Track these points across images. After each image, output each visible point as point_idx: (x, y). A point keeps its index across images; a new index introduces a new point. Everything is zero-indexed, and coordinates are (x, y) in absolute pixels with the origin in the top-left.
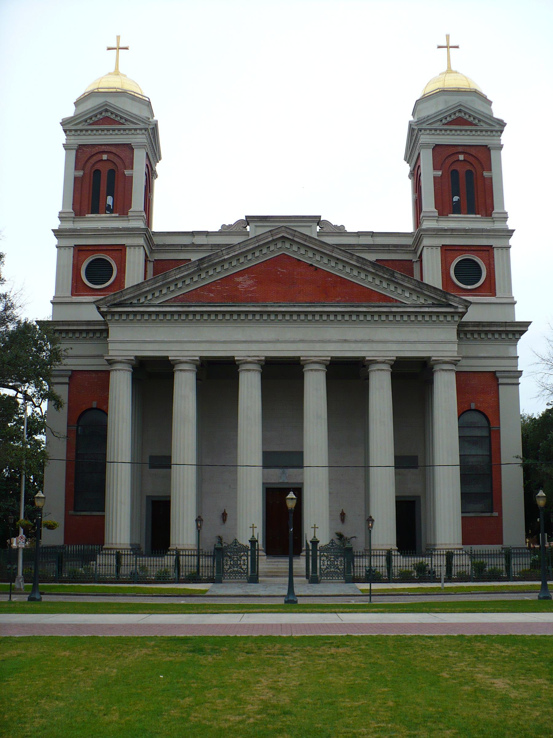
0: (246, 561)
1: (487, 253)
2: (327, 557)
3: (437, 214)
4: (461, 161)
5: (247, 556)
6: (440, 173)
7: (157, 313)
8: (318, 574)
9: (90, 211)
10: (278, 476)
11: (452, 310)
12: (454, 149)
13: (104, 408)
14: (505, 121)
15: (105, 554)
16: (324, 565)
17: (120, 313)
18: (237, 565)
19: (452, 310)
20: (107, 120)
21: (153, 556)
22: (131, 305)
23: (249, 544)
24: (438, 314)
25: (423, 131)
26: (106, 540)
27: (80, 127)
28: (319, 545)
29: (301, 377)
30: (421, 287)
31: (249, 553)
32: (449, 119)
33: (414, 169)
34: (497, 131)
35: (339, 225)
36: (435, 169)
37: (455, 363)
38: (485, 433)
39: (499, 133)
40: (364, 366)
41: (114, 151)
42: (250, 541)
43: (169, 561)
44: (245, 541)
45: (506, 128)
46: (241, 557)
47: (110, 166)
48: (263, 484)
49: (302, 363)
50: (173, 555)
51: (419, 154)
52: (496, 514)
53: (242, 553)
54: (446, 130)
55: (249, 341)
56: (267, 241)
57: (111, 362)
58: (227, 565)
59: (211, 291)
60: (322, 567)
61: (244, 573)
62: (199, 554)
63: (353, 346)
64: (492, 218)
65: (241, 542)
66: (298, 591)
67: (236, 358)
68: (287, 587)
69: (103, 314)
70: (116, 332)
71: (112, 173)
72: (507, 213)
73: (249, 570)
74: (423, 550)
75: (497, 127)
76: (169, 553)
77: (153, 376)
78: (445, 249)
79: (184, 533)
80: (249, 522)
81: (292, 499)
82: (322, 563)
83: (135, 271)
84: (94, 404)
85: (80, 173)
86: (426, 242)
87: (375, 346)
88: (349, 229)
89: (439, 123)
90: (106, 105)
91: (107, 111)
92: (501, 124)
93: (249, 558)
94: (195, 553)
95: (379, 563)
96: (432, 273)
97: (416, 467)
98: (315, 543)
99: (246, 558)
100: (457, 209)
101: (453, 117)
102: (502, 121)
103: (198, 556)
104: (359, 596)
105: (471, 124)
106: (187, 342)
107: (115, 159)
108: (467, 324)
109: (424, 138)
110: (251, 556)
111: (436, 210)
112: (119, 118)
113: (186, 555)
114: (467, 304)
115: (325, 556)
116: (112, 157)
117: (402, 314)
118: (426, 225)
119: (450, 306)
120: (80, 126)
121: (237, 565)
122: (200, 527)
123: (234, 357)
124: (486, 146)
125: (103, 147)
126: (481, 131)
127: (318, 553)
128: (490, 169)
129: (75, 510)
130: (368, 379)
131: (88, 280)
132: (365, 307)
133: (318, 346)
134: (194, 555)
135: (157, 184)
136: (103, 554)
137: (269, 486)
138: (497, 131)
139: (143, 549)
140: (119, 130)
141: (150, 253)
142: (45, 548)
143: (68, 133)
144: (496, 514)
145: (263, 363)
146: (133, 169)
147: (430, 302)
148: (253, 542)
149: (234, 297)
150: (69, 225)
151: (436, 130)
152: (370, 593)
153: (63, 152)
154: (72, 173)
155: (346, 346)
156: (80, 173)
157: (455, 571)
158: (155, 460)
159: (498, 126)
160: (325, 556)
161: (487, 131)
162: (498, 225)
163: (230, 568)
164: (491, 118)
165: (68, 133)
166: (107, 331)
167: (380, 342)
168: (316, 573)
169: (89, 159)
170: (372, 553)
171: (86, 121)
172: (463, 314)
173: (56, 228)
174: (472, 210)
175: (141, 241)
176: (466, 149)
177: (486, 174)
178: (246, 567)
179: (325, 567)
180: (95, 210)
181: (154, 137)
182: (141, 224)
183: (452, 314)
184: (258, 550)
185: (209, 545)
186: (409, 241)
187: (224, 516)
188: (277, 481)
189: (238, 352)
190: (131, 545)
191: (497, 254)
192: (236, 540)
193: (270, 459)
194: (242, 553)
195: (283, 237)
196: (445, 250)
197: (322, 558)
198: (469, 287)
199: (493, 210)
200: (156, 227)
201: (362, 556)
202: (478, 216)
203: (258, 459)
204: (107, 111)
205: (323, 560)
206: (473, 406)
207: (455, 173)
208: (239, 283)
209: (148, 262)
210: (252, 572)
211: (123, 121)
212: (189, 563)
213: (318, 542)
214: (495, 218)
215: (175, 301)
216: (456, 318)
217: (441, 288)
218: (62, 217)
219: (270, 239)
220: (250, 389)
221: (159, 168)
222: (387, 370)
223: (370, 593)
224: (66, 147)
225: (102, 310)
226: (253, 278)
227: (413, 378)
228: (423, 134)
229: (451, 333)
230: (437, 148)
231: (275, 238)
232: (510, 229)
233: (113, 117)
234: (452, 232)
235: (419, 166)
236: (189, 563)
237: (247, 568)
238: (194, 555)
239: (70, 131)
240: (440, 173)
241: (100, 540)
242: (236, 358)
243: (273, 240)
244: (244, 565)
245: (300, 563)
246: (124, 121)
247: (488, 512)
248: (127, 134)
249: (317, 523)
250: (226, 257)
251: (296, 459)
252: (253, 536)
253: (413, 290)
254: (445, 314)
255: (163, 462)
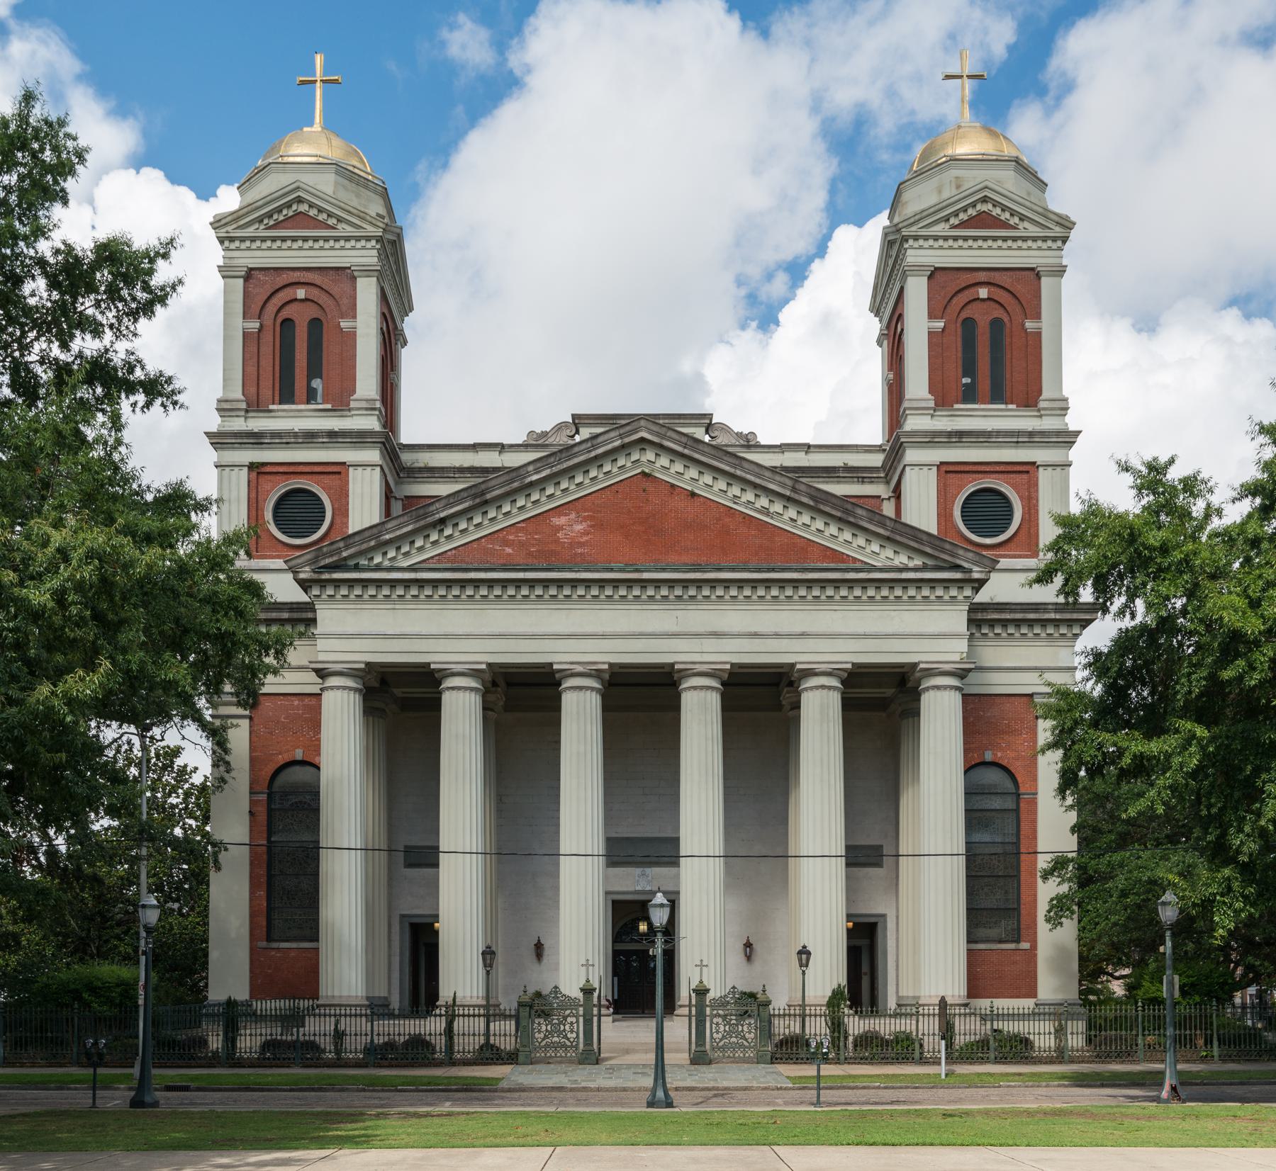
0: (574, 1028)
1: (1025, 476)
2: (724, 1017)
3: (932, 404)
4: (983, 300)
5: (577, 1017)
6: (940, 324)
7: (407, 584)
8: (708, 1046)
9: (277, 398)
10: (631, 881)
11: (958, 575)
12: (284, 279)
13: (316, 761)
14: (1072, 219)
15: (320, 1015)
16: (718, 1032)
17: (337, 583)
18: (560, 1033)
19: (958, 575)
20: (300, 220)
21: (415, 1018)
22: (357, 568)
23: (580, 995)
24: (933, 583)
25: (911, 242)
26: (322, 992)
27: (249, 232)
28: (711, 995)
29: (675, 707)
30: (900, 534)
31: (581, 1012)
32: (963, 216)
33: (888, 327)
34: (1054, 239)
35: (745, 432)
36: (932, 315)
37: (962, 674)
38: (1012, 805)
39: (1059, 243)
40: (791, 684)
41: (318, 283)
42: (582, 990)
43: (432, 1026)
44: (571, 987)
45: (1073, 234)
46: (565, 1018)
47: (313, 312)
48: (607, 893)
49: (676, 676)
50: (441, 1015)
51: (902, 289)
52: (1025, 945)
53: (568, 1012)
54: (955, 239)
55: (581, 634)
56: (610, 447)
57: (322, 674)
58: (539, 1032)
59: (506, 543)
60: (715, 1035)
61: (572, 1046)
62: (491, 1012)
63: (784, 644)
64: (1039, 410)
65: (567, 993)
66: (673, 1080)
67: (555, 667)
68: (652, 1072)
69: (305, 585)
70: (331, 617)
71: (316, 325)
72: (1066, 400)
73: (581, 1040)
74: (892, 1004)
75: (1058, 231)
76: (438, 1012)
77: (401, 700)
78: (947, 471)
79: (461, 977)
80: (578, 955)
81: (662, 905)
82: (716, 1030)
83: (364, 505)
84: (299, 754)
85: (254, 325)
86: (911, 455)
87: (810, 644)
88: (763, 440)
89: (942, 225)
90: (298, 188)
91: (299, 200)
92: (1066, 224)
93: (581, 1019)
94: (482, 1011)
95: (818, 1029)
96: (921, 506)
97: (879, 865)
98: (701, 992)
99: (574, 1020)
100: (969, 395)
101: (971, 212)
102: (1067, 218)
103: (488, 1018)
104: (786, 1089)
105: (1005, 225)
106: (462, 635)
107: (323, 299)
108: (984, 607)
109: (918, 255)
110: (584, 1016)
111: (930, 396)
112: (325, 216)
113: (469, 1016)
114: (992, 566)
115: (720, 1016)
116: (315, 293)
117: (865, 584)
118: (914, 423)
119: (957, 567)
120: (251, 229)
121: (560, 1033)
122: (491, 966)
123: (551, 664)
124: (1032, 269)
125: (297, 274)
126: (1025, 239)
127: (708, 1010)
128: (1038, 316)
129: (269, 939)
130: (799, 707)
131: (279, 529)
132: (796, 570)
133: (710, 644)
134: (479, 1016)
135: (408, 358)
136: (320, 1015)
137: (616, 670)
138: (1054, 239)
139: (395, 1004)
140: (326, 239)
141: (397, 483)
142: (215, 1005)
143: (227, 243)
144: (1025, 945)
145: (488, 677)
146: (355, 317)
147: (918, 562)
148: (587, 991)
149: (550, 559)
150: (238, 424)
151: (936, 238)
152: (819, 1083)
153: (220, 282)
154: (1045, 325)
155: (757, 645)
156: (254, 325)
157: (959, 1040)
158: (409, 850)
159: (1058, 229)
160: (720, 1016)
161: (1035, 239)
162: (1048, 424)
163: (546, 1037)
164: (1046, 213)
165: (227, 243)
166: (313, 621)
167: (823, 636)
168: (704, 1044)
169: (269, 298)
170: (808, 1012)
171: (260, 220)
172: (981, 583)
173: (214, 428)
174: (998, 395)
175: (374, 455)
176: (990, 276)
177: (1029, 325)
178: (574, 1035)
179: (720, 1035)
180: (287, 396)
181: (397, 263)
182: (372, 423)
183: (960, 584)
184: (600, 1006)
185: (508, 1003)
186: (877, 460)
187: (539, 949)
188: (631, 889)
189: (559, 655)
190: (368, 998)
191: (1044, 476)
192: (556, 987)
193: (620, 851)
194: (568, 1012)
195: (643, 440)
196: (947, 472)
197: (715, 1020)
198: (988, 541)
199: (1040, 394)
200: (409, 433)
201: (784, 1015)
202: (1010, 406)
203: (596, 844)
204: (299, 200)
205: (717, 1024)
206: (989, 756)
207: (969, 324)
208: (560, 528)
209: (393, 501)
210: (585, 1045)
211: (332, 221)
212: (470, 1032)
213: (708, 991)
214: (1045, 409)
215: (439, 562)
216: (968, 592)
217: (935, 533)
218: (225, 408)
219: (617, 443)
220: (461, 717)
221: (410, 325)
222: (834, 688)
223: (819, 1083)
224: (226, 271)
225: (302, 576)
226: (585, 519)
227: (881, 702)
228: (911, 247)
229: (955, 619)
230: (935, 274)
231: (627, 440)
232: (1071, 429)
233: (313, 212)
234: (959, 437)
235: (900, 316)
236: (470, 1032)
237: (578, 1036)
238: (479, 1016)
239: (232, 239)
240: (940, 324)
241: (312, 990)
242: (555, 667)
243: (623, 447)
244: (572, 1031)
245: (678, 1030)
246: (335, 221)
247: (1012, 942)
248: (342, 248)
249: (705, 955)
250: (535, 478)
251: (665, 851)
252: (588, 981)
253: (888, 539)
254: (946, 583)
255: (424, 857)
